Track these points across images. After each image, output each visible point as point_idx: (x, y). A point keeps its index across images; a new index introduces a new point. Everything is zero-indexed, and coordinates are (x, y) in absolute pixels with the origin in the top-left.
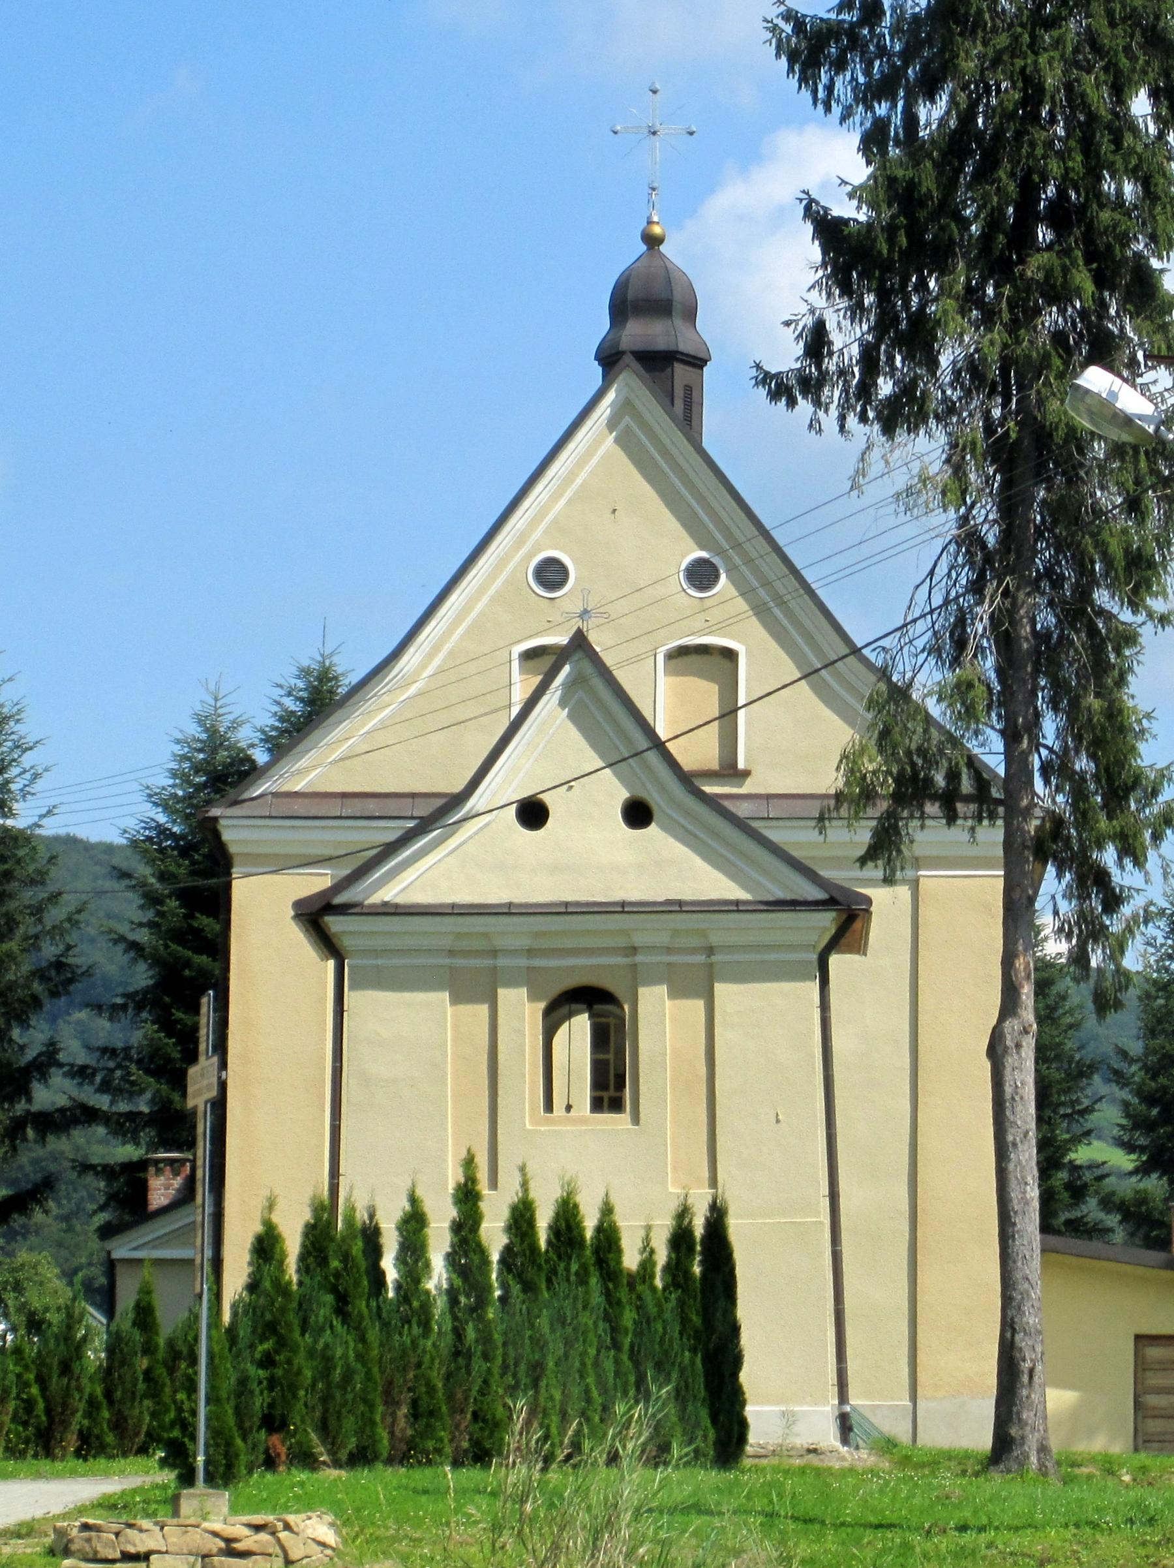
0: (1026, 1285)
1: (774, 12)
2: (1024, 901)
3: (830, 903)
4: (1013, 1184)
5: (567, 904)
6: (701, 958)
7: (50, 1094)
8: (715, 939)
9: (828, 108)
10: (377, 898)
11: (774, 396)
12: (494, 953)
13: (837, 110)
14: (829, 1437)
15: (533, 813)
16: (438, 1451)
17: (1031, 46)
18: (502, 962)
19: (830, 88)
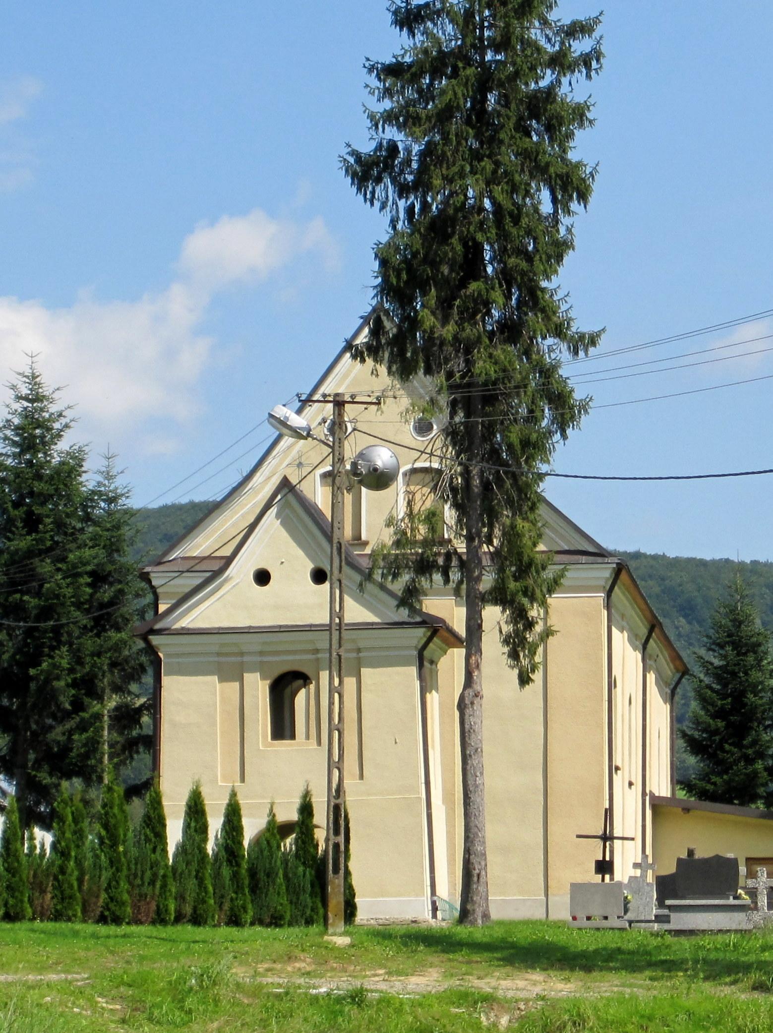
0: (476, 830)
1: (344, 151)
2: (476, 627)
3: (423, 623)
4: (469, 776)
5: (280, 626)
6: (354, 655)
8: (361, 645)
9: (372, 204)
10: (177, 626)
12: (242, 654)
13: (377, 204)
14: (428, 915)
15: (263, 577)
16: (75, 916)
17: (471, 172)
18: (246, 659)
19: (373, 193)
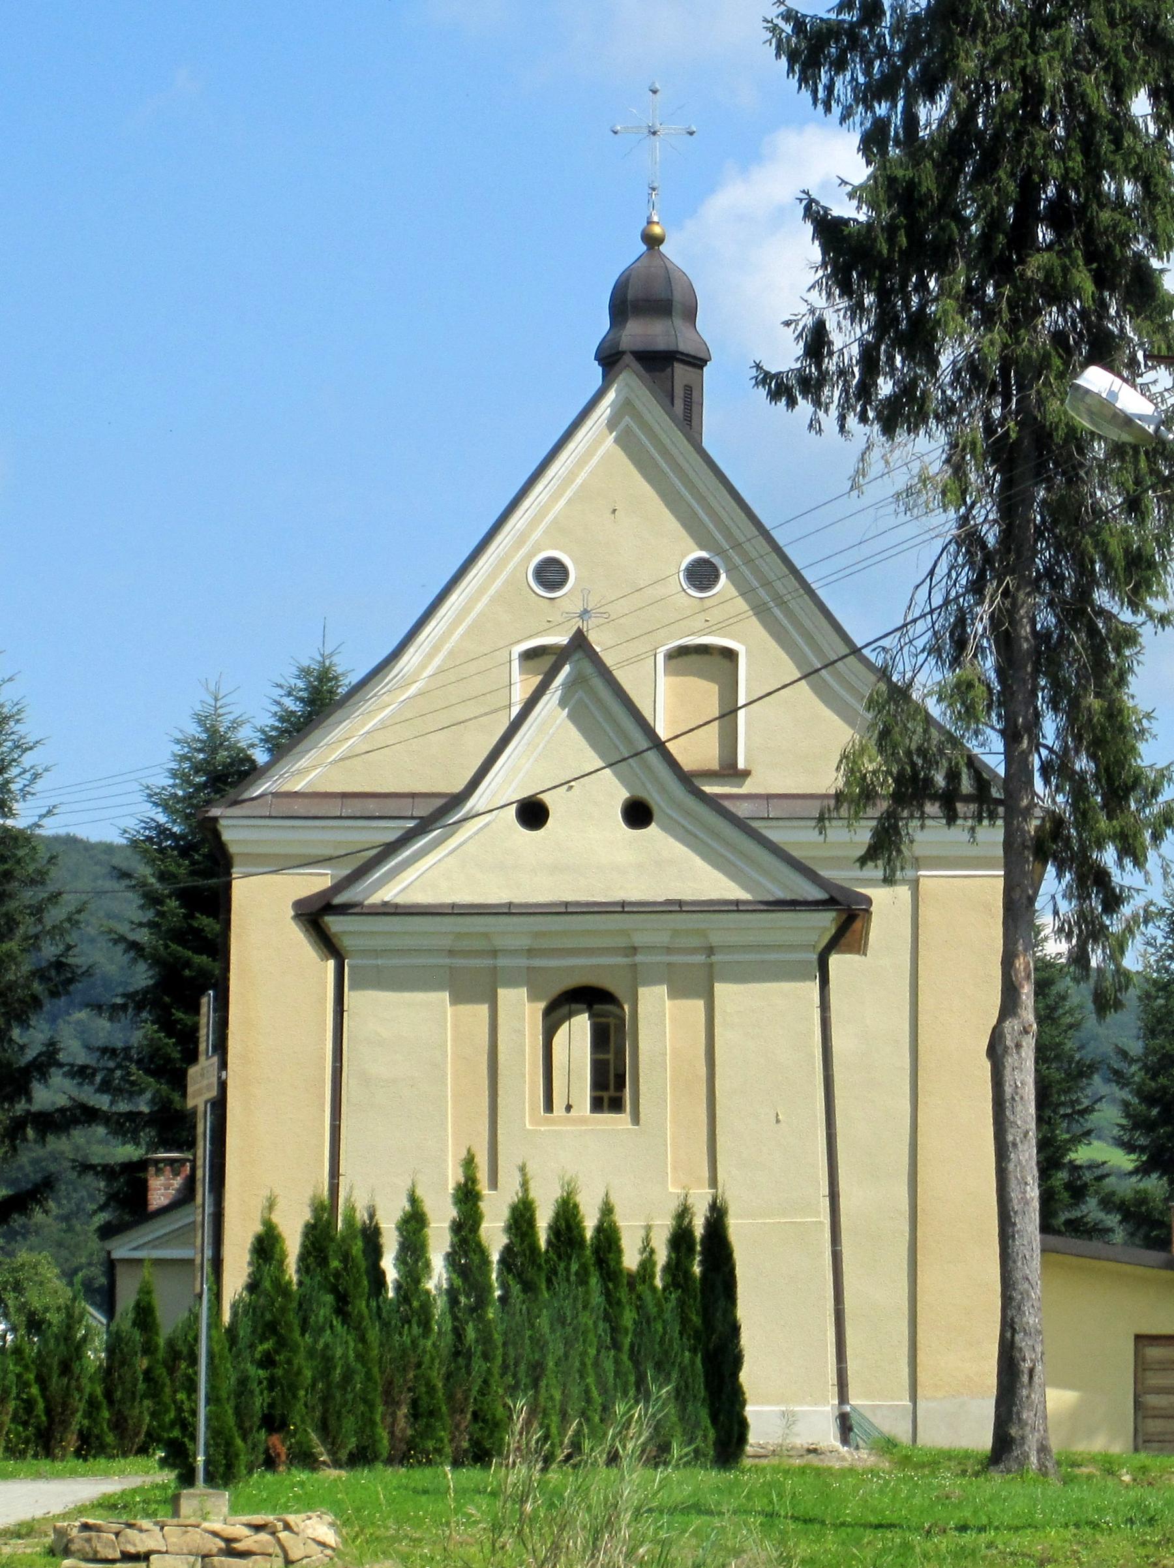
0: (1026, 1285)
1: (774, 12)
2: (1024, 901)
3: (830, 903)
4: (1013, 1184)
5: (567, 904)
6: (701, 958)
7: (50, 1094)
8: (715, 939)
9: (828, 108)
10: (377, 898)
11: (774, 396)
12: (494, 953)
13: (837, 110)
14: (829, 1437)
15: (533, 813)
16: (438, 1451)
18: (502, 962)
19: (830, 88)
